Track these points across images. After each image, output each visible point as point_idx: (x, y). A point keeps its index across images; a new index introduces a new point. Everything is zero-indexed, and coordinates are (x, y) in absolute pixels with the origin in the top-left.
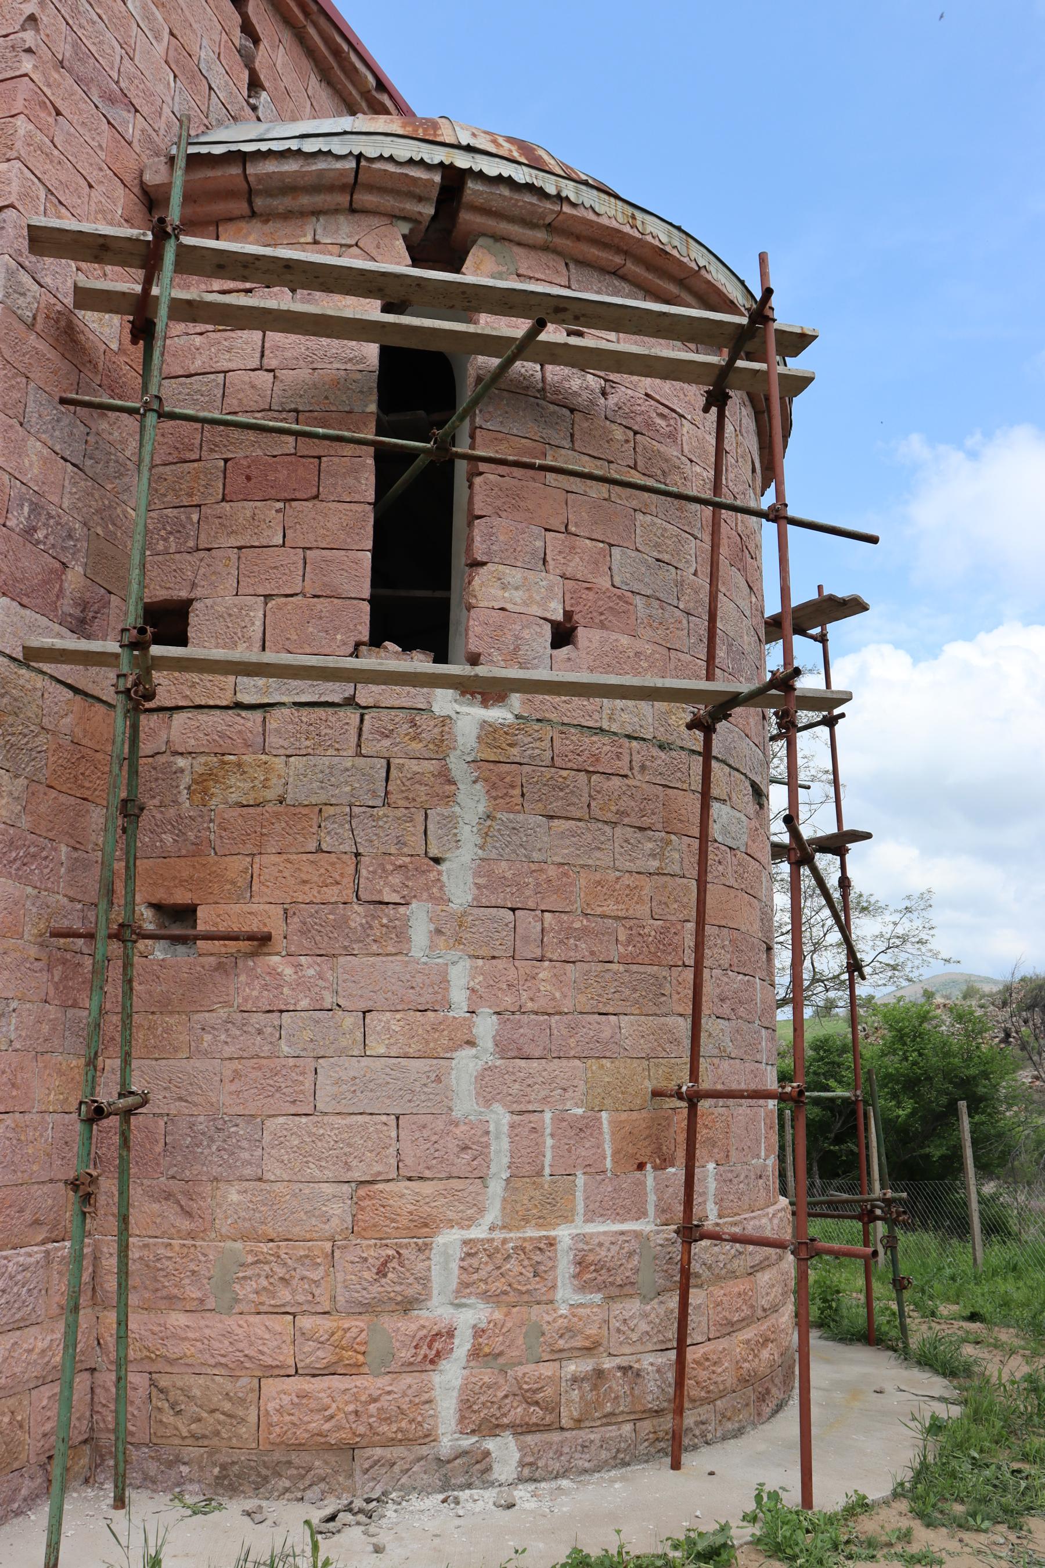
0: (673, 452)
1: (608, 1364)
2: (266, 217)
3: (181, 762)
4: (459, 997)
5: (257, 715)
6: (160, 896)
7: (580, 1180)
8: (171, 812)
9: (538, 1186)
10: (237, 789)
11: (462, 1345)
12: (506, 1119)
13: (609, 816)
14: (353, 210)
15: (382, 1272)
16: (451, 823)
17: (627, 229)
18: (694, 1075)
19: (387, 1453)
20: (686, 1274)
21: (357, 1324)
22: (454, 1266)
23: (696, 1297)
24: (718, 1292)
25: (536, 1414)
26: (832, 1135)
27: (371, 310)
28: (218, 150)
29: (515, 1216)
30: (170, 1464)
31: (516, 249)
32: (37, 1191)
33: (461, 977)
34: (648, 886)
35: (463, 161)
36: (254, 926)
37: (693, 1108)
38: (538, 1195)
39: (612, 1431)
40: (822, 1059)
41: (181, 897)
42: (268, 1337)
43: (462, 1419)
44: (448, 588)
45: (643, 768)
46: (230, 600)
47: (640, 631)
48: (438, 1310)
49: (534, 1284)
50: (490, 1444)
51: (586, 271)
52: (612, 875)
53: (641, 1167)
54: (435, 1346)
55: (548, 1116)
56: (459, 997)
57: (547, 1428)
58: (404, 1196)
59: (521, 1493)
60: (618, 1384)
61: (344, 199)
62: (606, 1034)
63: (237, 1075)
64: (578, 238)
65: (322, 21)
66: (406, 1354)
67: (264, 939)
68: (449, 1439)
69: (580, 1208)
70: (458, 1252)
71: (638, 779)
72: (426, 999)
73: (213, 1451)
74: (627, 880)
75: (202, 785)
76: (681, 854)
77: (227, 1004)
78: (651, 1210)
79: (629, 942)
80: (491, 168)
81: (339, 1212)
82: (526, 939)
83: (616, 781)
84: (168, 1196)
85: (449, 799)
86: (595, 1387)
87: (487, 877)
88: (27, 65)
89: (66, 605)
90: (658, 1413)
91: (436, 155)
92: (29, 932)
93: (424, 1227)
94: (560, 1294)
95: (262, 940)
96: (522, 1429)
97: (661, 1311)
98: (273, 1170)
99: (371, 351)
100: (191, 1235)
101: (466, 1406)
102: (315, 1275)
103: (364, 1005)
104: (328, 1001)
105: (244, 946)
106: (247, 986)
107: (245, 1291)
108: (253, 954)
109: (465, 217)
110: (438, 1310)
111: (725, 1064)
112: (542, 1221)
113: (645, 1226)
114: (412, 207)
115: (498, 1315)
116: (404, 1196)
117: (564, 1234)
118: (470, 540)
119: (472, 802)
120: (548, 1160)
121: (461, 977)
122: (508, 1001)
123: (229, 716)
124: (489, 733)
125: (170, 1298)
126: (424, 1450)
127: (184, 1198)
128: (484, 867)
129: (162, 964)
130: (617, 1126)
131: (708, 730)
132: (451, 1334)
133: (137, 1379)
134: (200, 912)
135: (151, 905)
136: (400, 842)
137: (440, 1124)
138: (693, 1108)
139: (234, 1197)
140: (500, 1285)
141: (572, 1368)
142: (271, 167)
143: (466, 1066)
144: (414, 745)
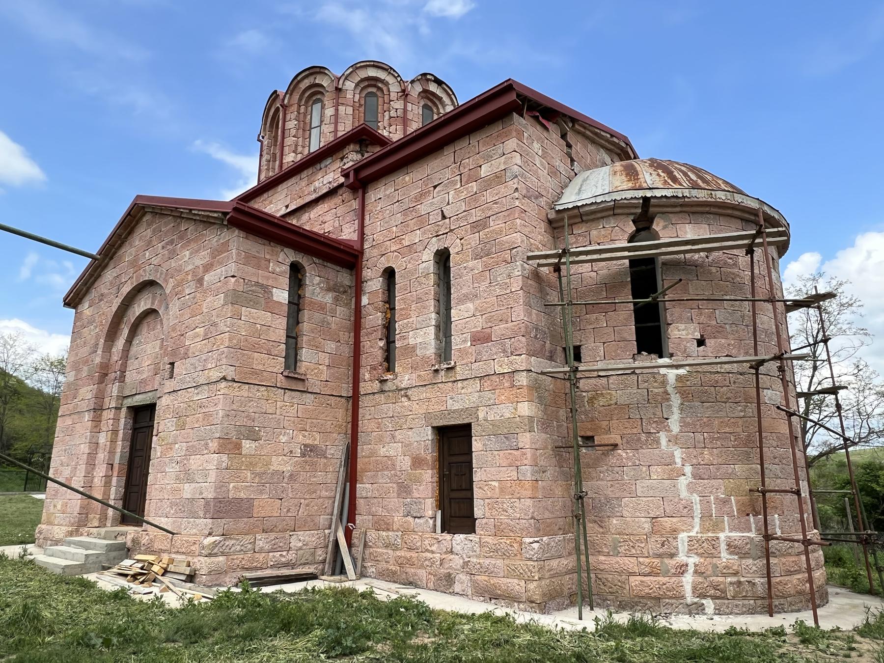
0: (736, 270)
1: (742, 579)
2: (587, 222)
3: (584, 394)
4: (678, 460)
5: (606, 379)
6: (583, 434)
7: (726, 518)
8: (583, 409)
9: (711, 520)
10: (602, 401)
11: (691, 569)
12: (698, 498)
13: (723, 400)
14: (614, 215)
15: (663, 545)
16: (670, 406)
17: (710, 199)
18: (763, 485)
19: (670, 601)
20: (767, 550)
21: (656, 561)
22: (686, 544)
23: (773, 560)
24: (784, 560)
25: (718, 593)
26: (879, 511)
27: (626, 254)
28: (570, 206)
29: (704, 530)
30: (604, 601)
31: (670, 215)
32: (560, 520)
33: (678, 454)
34: (740, 422)
35: (649, 194)
36: (612, 442)
37: (764, 495)
38: (711, 523)
39: (746, 602)
40: (868, 474)
41: (589, 434)
42: (630, 563)
43: (693, 592)
44: (659, 321)
45: (735, 382)
46: (593, 345)
47: (729, 336)
48: (682, 558)
49: (713, 551)
50: (704, 601)
51: (696, 215)
52: (727, 419)
53: (748, 515)
54: (682, 569)
55: (712, 498)
56: (678, 460)
57: (723, 598)
58: (668, 523)
59: (716, 617)
60: (747, 587)
61: (611, 213)
62: (730, 471)
63: (612, 486)
64: (692, 206)
65: (591, 128)
66: (673, 571)
67: (616, 445)
68: (690, 598)
69: (727, 527)
70: (687, 540)
71: (733, 386)
72: (668, 461)
73: (617, 597)
74: (732, 420)
75: (591, 400)
76: (752, 409)
77: (606, 465)
78: (753, 530)
79: (735, 440)
80: (658, 193)
81: (647, 526)
82: (699, 442)
83: (725, 388)
84: (595, 522)
85: (668, 400)
86: (738, 587)
87: (684, 424)
88: (517, 203)
89: (547, 354)
90: (763, 598)
91: (640, 194)
92: (550, 447)
93: (675, 531)
94: (722, 555)
95: (615, 446)
96: (714, 598)
97: (761, 564)
98: (625, 513)
99: (627, 262)
100: (603, 533)
101: (694, 589)
102: (643, 545)
103: (648, 464)
104: (637, 463)
105: (610, 448)
106: (612, 460)
107: (621, 550)
108: (613, 450)
109: (652, 210)
110: (682, 558)
111: (779, 481)
112: (714, 531)
113: (752, 535)
114: (633, 211)
115: (702, 560)
116: (668, 523)
117: (722, 536)
118: (666, 317)
119: (676, 400)
120: (714, 512)
121: (678, 454)
122: (695, 461)
123: (598, 380)
124: (679, 378)
125: (599, 552)
126: (682, 601)
127: (600, 523)
128: (682, 420)
129: (586, 454)
130: (737, 502)
131: (757, 370)
132: (687, 565)
133: (592, 576)
134: (595, 438)
135: (582, 437)
136: (654, 414)
137: (676, 500)
138: (764, 495)
139: (615, 522)
140: (702, 551)
141: (729, 579)
142: (587, 209)
143: (683, 482)
144: (655, 384)
